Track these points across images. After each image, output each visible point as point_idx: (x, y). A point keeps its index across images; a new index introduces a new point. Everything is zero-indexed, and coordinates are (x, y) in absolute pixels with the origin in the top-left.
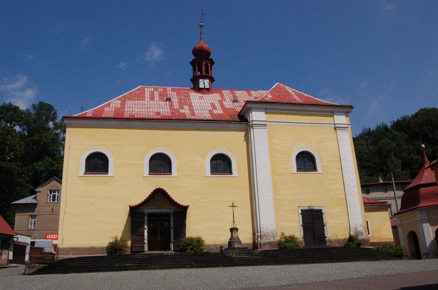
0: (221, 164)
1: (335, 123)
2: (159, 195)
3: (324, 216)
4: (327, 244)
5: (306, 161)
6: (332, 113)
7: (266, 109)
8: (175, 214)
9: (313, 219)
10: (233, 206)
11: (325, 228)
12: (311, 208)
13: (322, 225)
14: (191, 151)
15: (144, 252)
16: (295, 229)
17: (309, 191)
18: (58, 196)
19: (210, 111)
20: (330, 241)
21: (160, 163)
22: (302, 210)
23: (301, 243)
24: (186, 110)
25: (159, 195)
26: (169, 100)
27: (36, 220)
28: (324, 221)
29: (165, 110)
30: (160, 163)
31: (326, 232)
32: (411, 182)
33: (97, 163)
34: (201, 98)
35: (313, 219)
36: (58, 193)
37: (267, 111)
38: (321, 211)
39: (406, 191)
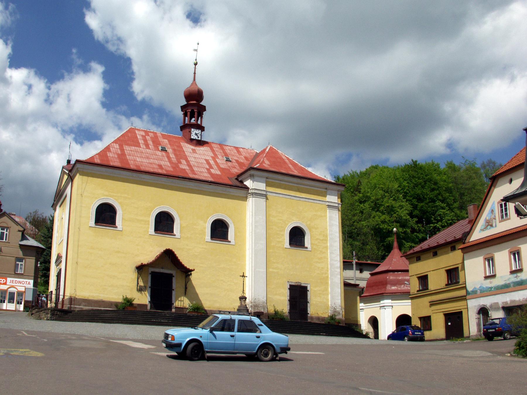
0: (219, 230)
2: (169, 255)
3: (308, 292)
4: (309, 321)
5: (297, 237)
6: (325, 190)
7: (267, 178)
9: (298, 294)
10: (243, 276)
11: (308, 305)
13: (306, 302)
14: (194, 213)
16: (281, 303)
17: (295, 267)
18: (6, 234)
19: (207, 169)
20: (312, 318)
21: (164, 223)
22: (290, 285)
23: (287, 316)
24: (184, 166)
25: (169, 255)
26: (164, 150)
27: (23, 263)
28: (309, 298)
29: (166, 166)
30: (164, 223)
31: (309, 309)
32: (379, 265)
33: (106, 215)
34: (194, 151)
35: (298, 294)
36: (7, 231)
37: (267, 180)
38: (306, 288)
39: (372, 275)
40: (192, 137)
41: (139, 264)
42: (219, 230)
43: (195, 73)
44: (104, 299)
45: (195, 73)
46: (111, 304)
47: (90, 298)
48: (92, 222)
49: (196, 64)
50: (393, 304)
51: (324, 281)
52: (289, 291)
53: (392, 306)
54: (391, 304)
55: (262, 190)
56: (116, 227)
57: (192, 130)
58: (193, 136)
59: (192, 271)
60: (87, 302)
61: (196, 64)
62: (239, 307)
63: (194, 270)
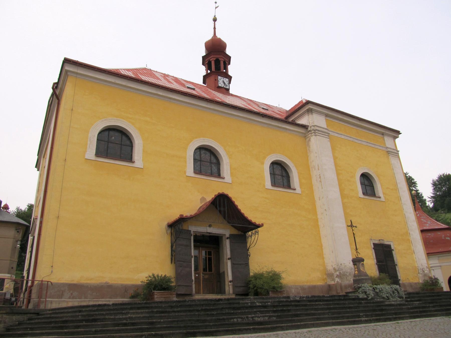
0: (280, 174)
1: (387, 146)
3: (394, 252)
8: (232, 237)
12: (382, 242)
15: (190, 295)
21: (207, 161)
25: (222, 205)
28: (395, 259)
30: (207, 161)
40: (220, 85)
41: (175, 216)
42: (280, 174)
43: (215, 28)
44: (111, 282)
45: (215, 28)
46: (125, 289)
47: (83, 281)
48: (91, 152)
49: (215, 20)
50: (441, 264)
51: (405, 237)
52: (373, 251)
53: (441, 266)
54: (439, 265)
55: (324, 128)
56: (134, 162)
57: (219, 77)
58: (221, 84)
59: (258, 226)
60: (76, 288)
61: (215, 20)
62: (355, 276)
63: (262, 225)
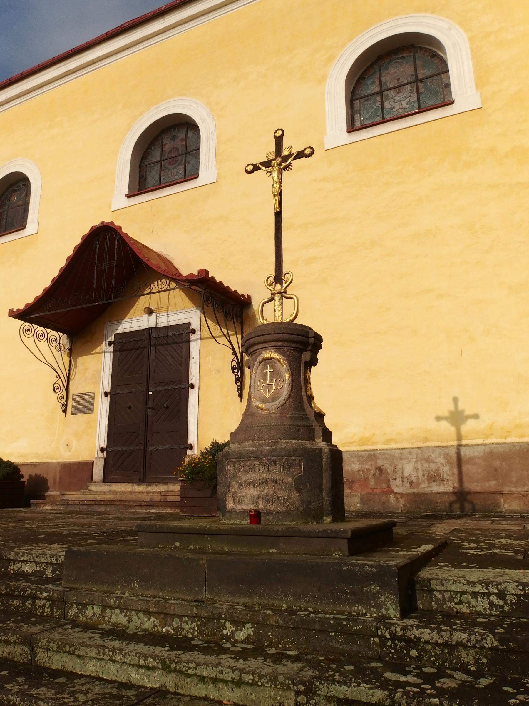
30: (166, 152)
